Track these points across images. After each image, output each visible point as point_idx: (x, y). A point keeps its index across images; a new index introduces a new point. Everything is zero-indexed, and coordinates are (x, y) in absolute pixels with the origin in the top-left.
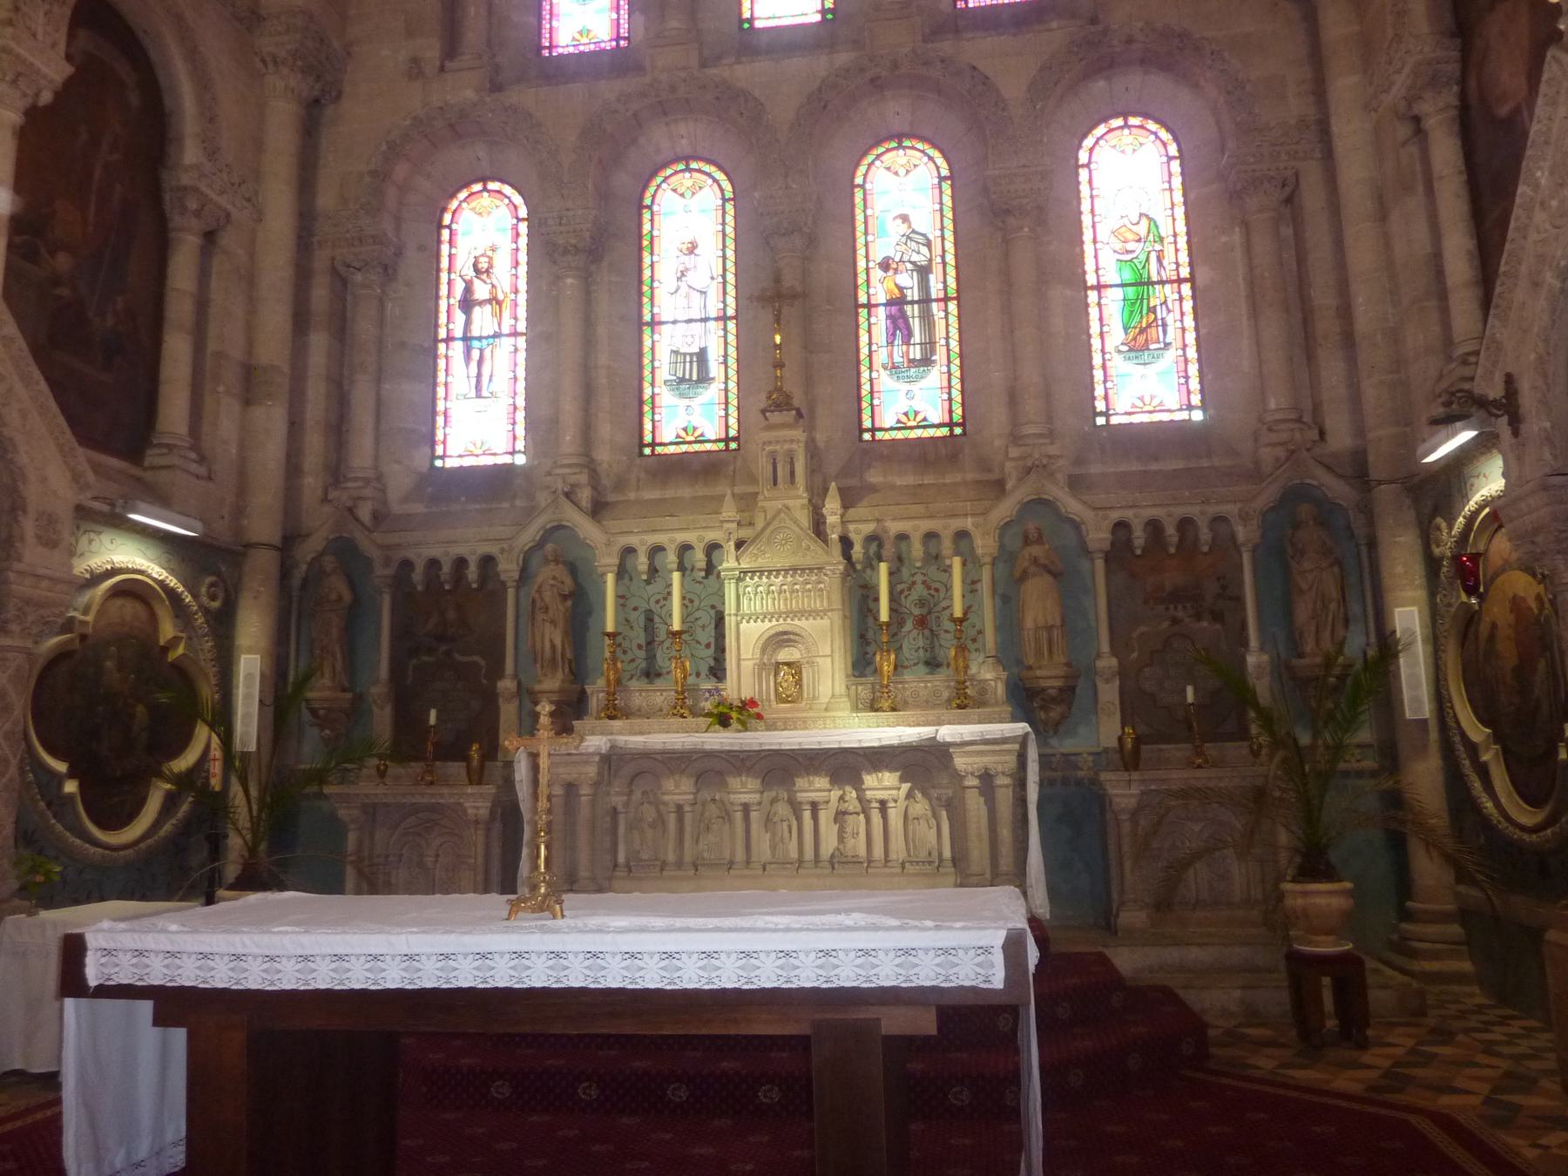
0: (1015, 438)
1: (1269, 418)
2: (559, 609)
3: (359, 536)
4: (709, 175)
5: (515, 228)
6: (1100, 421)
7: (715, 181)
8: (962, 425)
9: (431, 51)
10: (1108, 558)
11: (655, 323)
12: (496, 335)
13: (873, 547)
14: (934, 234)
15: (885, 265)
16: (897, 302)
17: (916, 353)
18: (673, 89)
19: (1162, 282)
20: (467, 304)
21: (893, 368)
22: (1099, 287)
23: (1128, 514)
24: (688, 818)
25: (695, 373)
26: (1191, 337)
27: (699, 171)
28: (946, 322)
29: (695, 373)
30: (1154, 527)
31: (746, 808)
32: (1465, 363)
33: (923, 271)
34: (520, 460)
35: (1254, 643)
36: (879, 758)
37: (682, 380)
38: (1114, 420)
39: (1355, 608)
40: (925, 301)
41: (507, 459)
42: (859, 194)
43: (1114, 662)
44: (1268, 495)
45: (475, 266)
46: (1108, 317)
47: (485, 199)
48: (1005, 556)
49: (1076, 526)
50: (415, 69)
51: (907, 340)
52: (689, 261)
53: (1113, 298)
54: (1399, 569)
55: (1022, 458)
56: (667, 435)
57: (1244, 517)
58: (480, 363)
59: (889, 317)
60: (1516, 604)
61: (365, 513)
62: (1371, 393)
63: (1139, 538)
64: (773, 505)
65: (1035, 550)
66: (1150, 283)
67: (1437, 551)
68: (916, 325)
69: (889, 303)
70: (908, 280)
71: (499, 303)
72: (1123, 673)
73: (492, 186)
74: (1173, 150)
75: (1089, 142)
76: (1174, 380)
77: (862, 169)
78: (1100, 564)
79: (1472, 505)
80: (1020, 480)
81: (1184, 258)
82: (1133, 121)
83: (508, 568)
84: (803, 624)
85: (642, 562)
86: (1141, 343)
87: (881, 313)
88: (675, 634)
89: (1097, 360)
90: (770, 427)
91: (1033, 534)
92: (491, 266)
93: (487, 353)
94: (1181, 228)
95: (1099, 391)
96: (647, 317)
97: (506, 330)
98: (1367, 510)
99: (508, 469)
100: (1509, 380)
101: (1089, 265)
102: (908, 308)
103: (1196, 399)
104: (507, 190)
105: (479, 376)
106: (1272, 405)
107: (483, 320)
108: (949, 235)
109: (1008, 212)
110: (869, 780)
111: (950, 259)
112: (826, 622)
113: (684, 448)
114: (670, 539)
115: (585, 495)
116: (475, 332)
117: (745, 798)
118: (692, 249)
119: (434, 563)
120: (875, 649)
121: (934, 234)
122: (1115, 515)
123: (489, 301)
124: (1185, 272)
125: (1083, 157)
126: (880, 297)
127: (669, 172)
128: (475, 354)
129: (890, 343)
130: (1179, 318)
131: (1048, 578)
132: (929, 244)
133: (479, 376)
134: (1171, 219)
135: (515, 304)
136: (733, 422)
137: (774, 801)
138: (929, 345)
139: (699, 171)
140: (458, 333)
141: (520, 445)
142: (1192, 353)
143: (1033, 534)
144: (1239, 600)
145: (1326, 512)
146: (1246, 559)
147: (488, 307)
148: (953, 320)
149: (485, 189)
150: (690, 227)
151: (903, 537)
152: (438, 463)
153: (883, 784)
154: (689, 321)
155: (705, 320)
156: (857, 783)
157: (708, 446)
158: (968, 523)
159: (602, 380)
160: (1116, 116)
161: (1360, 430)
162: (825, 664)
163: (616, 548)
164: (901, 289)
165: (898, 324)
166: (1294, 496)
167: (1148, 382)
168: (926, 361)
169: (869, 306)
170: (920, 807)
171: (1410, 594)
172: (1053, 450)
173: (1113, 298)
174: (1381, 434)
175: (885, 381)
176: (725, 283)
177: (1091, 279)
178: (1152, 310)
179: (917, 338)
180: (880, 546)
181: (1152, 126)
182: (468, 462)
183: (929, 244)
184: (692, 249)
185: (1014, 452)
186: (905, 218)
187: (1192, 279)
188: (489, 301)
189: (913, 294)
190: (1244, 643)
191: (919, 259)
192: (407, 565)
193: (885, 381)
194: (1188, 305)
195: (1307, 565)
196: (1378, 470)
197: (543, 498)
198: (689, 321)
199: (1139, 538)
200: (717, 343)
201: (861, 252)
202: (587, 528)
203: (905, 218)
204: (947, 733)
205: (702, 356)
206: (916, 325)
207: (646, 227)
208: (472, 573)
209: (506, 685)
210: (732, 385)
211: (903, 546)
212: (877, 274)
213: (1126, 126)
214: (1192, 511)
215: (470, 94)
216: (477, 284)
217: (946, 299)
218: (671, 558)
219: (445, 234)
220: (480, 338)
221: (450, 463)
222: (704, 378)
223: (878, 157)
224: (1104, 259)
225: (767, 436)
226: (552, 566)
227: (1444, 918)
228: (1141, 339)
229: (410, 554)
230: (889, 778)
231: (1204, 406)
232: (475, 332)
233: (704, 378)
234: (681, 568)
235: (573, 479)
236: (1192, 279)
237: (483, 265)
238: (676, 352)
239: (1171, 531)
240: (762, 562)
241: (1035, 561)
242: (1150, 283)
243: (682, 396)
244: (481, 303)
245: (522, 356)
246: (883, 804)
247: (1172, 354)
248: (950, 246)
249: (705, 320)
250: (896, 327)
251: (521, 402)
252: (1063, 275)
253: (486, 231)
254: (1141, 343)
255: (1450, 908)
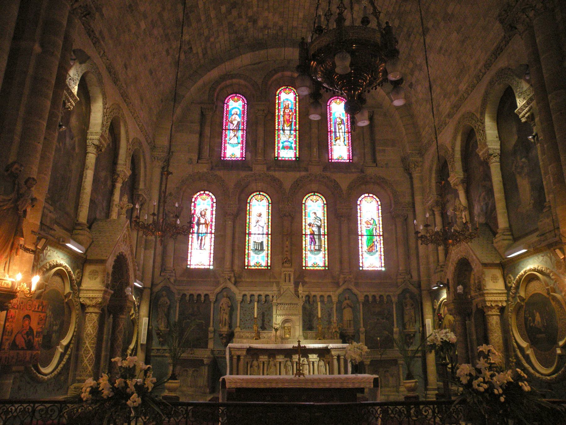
0: (341, 272)
1: (400, 272)
2: (227, 310)
3: (171, 286)
4: (265, 196)
5: (212, 205)
6: (361, 269)
7: (267, 198)
8: (328, 267)
9: (195, 157)
10: (364, 304)
11: (250, 234)
12: (207, 233)
13: (307, 298)
14: (322, 218)
15: (310, 225)
16: (313, 234)
17: (317, 248)
18: (260, 176)
19: (376, 236)
20: (199, 224)
21: (311, 251)
22: (362, 235)
23: (368, 294)
24: (266, 365)
25: (260, 248)
26: (382, 249)
27: (263, 195)
28: (324, 240)
29: (260, 248)
30: (374, 296)
31: (280, 363)
32: (441, 267)
33: (319, 227)
34: (211, 267)
35: (395, 326)
36: (313, 351)
37: (256, 249)
38: (364, 269)
39: (417, 318)
40: (319, 235)
41: (208, 267)
42: (303, 206)
43: (364, 329)
44: (399, 291)
45: (201, 213)
46: (363, 244)
47: (204, 196)
48: (340, 302)
49: (356, 295)
50: (190, 161)
51: (315, 245)
52: (259, 219)
53: (365, 239)
54: (427, 310)
55: (345, 278)
56: (252, 264)
57: (394, 296)
58: (201, 240)
59: (311, 238)
60: (449, 321)
61: (172, 280)
62: (422, 269)
63: (371, 299)
64: (285, 287)
65: (347, 301)
66: (373, 235)
67: (435, 307)
68: (317, 240)
69: (311, 234)
70: (315, 229)
71: (207, 225)
72: (366, 332)
73: (207, 192)
74: (379, 203)
75: (360, 199)
76: (379, 260)
77: (305, 199)
78: (361, 305)
79: (441, 299)
80: (344, 283)
81: (381, 230)
82: (371, 195)
83: (212, 298)
84: (293, 318)
85: (248, 299)
86: (371, 250)
87: (309, 236)
88: (255, 318)
89: (360, 253)
90: (285, 267)
91: (347, 298)
92: (205, 214)
93: (203, 238)
94: (381, 222)
95: (361, 261)
96: (247, 232)
97: (209, 232)
98: (420, 295)
99: (208, 270)
100: (448, 280)
101: (359, 230)
102: (315, 236)
103: (383, 265)
104: (211, 194)
105: (201, 243)
106: (401, 269)
107: (203, 229)
108: (326, 218)
109: (342, 216)
110: (310, 356)
111: (326, 224)
112: (298, 317)
113: (256, 267)
114: (256, 293)
115: (233, 280)
116: (200, 232)
117: (280, 360)
118: (260, 215)
119: (191, 295)
120: (308, 326)
121: (322, 218)
122: (365, 294)
123: (204, 224)
124: (381, 234)
125: (359, 203)
126: (308, 232)
127: (255, 194)
128: (200, 238)
129: (311, 245)
130: (380, 246)
131: (350, 309)
132: (321, 221)
133: (201, 243)
134: (378, 220)
135: (211, 225)
136: (269, 261)
137: (286, 361)
138: (320, 246)
139: (263, 195)
140: (196, 231)
141: (212, 263)
142: (382, 254)
143: (347, 298)
144: (392, 316)
145: (412, 297)
146: (394, 306)
147: (204, 225)
148: (326, 240)
149: (204, 193)
150: (259, 211)
151: (315, 296)
152: (189, 266)
153: (313, 357)
154: (259, 234)
155: (263, 234)
156: (307, 357)
157: (263, 268)
158: (331, 294)
159: (236, 248)
160: (366, 193)
161: (419, 276)
162: (297, 327)
163: (242, 294)
164: (313, 231)
165: (313, 240)
166: (405, 291)
167: (372, 261)
168: (319, 250)
169: (306, 235)
170: (322, 363)
171: (429, 316)
172: (351, 276)
173: (365, 239)
174: (424, 278)
175: (309, 254)
176: (268, 226)
177: (360, 233)
178: (374, 242)
179: (317, 244)
180: (309, 298)
181: (375, 197)
182: (197, 267)
183: (321, 221)
184: (260, 215)
185: (342, 276)
186: (315, 213)
187: (383, 235)
188: (204, 224)
189: (316, 233)
190: (393, 325)
191: (319, 224)
192: (184, 295)
193: (309, 254)
194: (382, 242)
195: (408, 308)
196: (423, 286)
197: (221, 280)
198: (259, 234)
199: (371, 299)
200: (265, 240)
201: (304, 220)
202: (233, 288)
203: (315, 213)
204: (331, 346)
205: (262, 243)
206: (317, 240)
207: (248, 208)
208: (203, 298)
209: (211, 329)
210: (269, 252)
211: (315, 298)
212: (308, 227)
213: (369, 196)
214: (382, 293)
215: (205, 170)
216: (201, 219)
217: (324, 235)
218: (256, 298)
219: (193, 204)
220: (201, 233)
221: (192, 267)
222: (262, 249)
223: (309, 197)
224: (363, 228)
225: (284, 269)
226: (225, 298)
227: (434, 390)
228: (371, 249)
229: (186, 292)
230: (315, 356)
231: (385, 267)
232: (200, 232)
233: (262, 249)
234: (258, 302)
235: (229, 275)
236: (383, 235)
237: (203, 213)
238: (255, 242)
239: (378, 298)
240: (282, 301)
241: (347, 304)
242: (373, 235)
243: (256, 254)
244: (202, 224)
245: (213, 239)
246: (313, 362)
247: (378, 253)
248: (326, 221)
249: (263, 234)
250: (312, 241)
251: (212, 252)
252: (353, 233)
253: (204, 205)
254: (371, 250)
255: (436, 387)
